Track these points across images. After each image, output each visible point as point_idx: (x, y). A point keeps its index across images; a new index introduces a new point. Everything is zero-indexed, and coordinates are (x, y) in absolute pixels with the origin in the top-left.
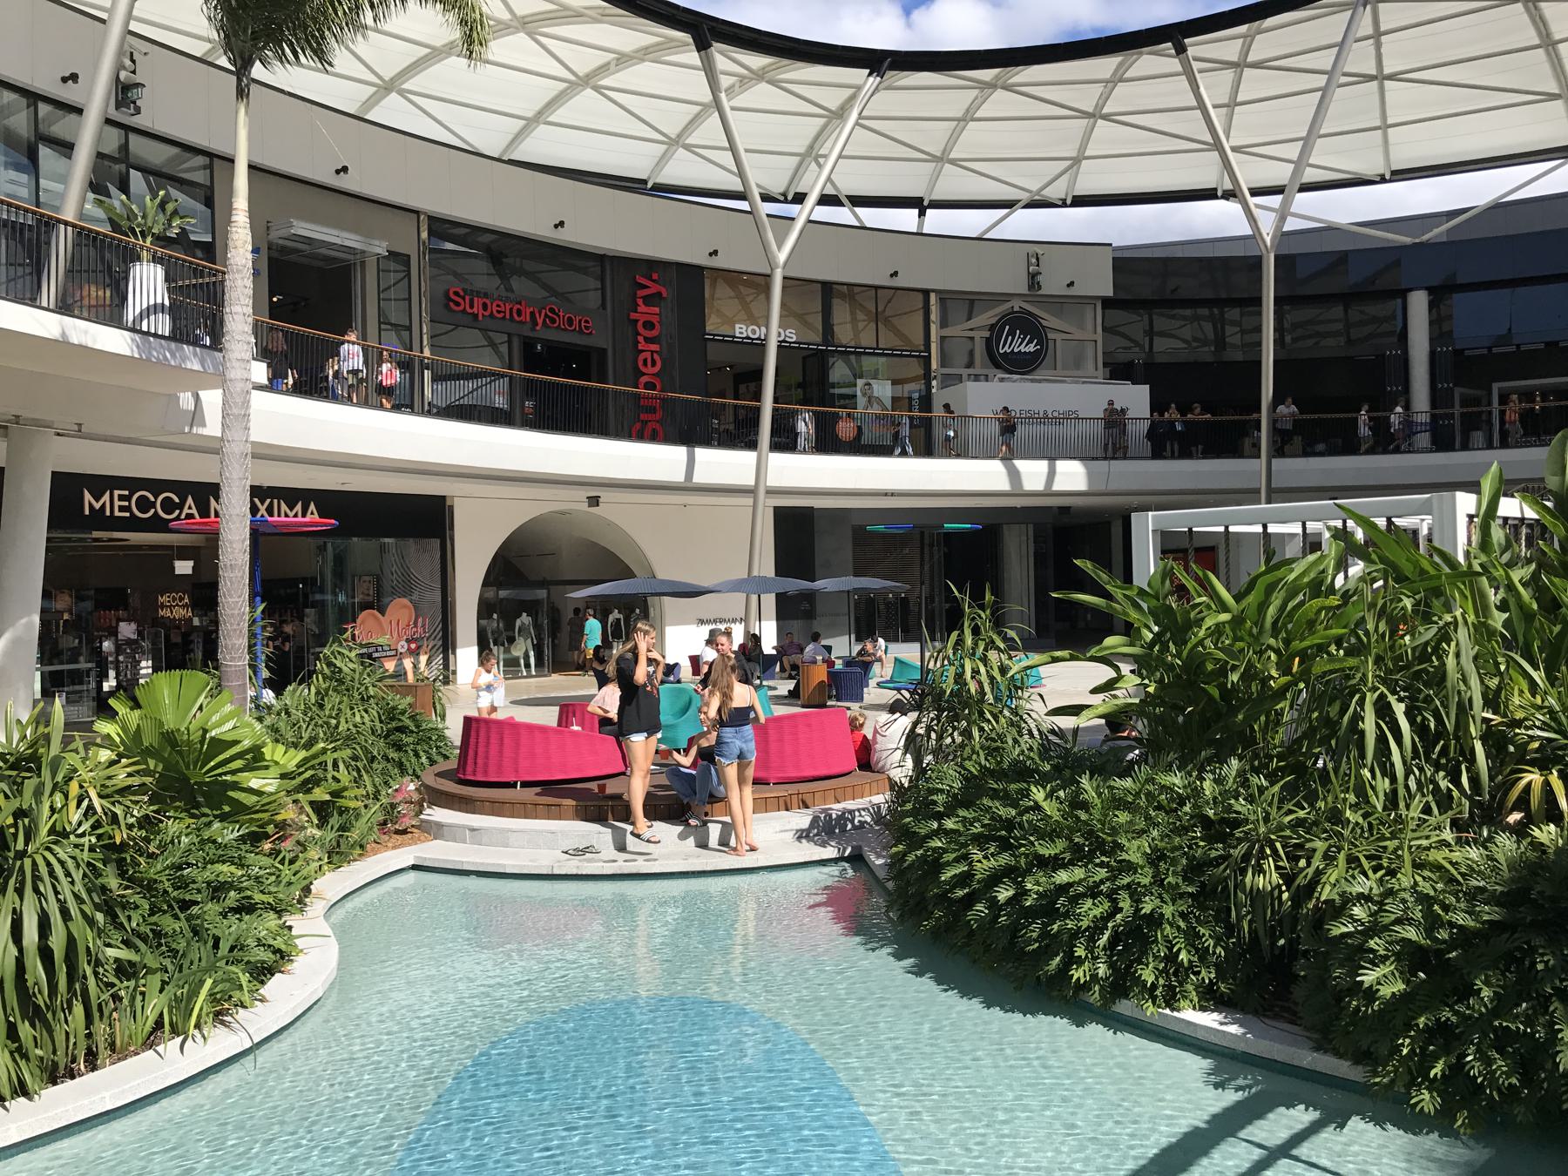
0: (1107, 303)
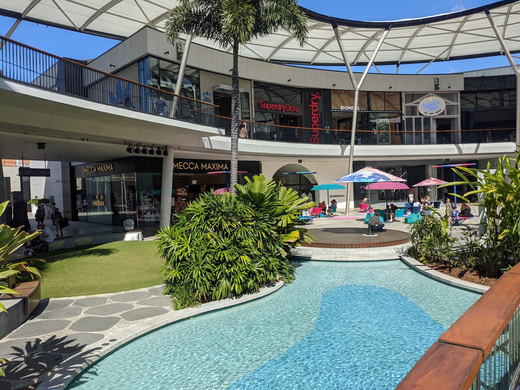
0: (461, 92)
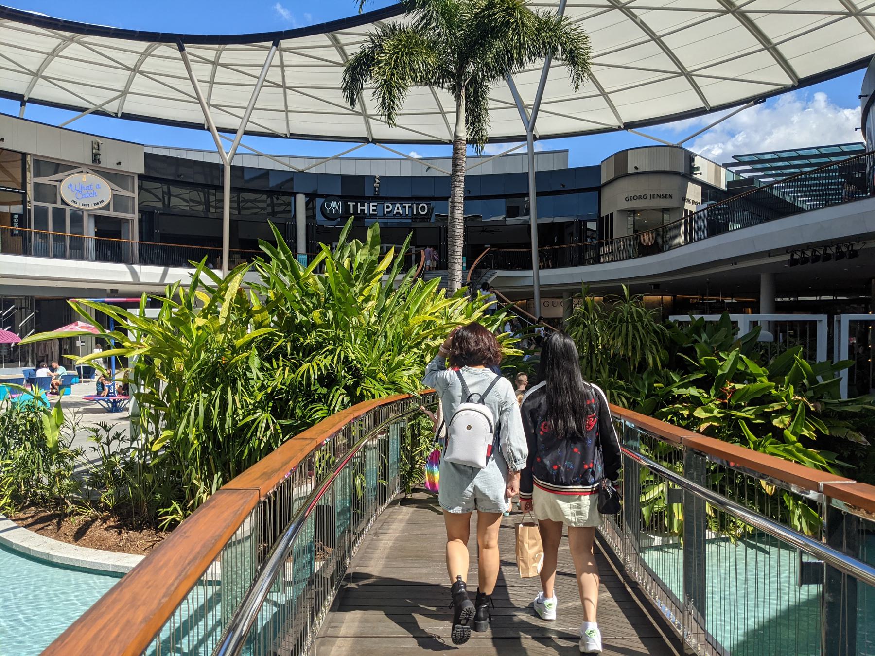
0: (140, 177)
